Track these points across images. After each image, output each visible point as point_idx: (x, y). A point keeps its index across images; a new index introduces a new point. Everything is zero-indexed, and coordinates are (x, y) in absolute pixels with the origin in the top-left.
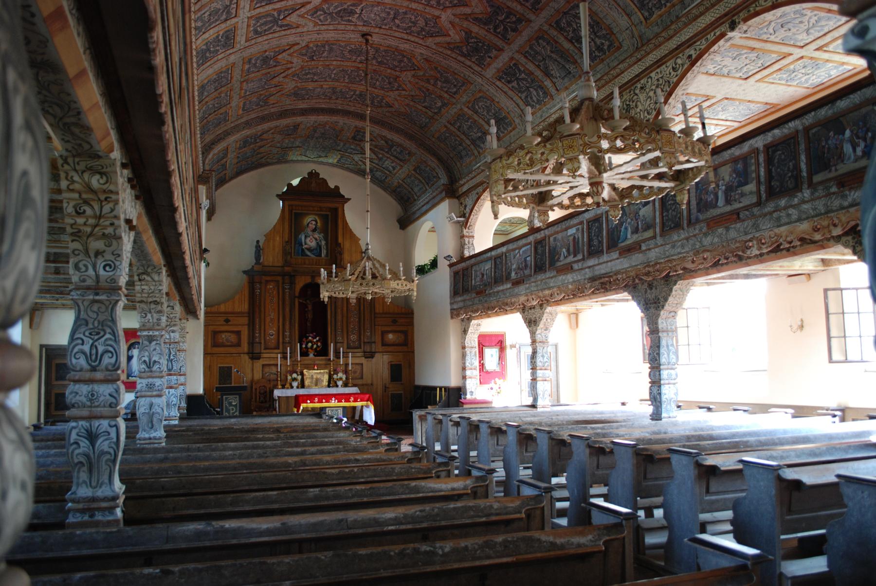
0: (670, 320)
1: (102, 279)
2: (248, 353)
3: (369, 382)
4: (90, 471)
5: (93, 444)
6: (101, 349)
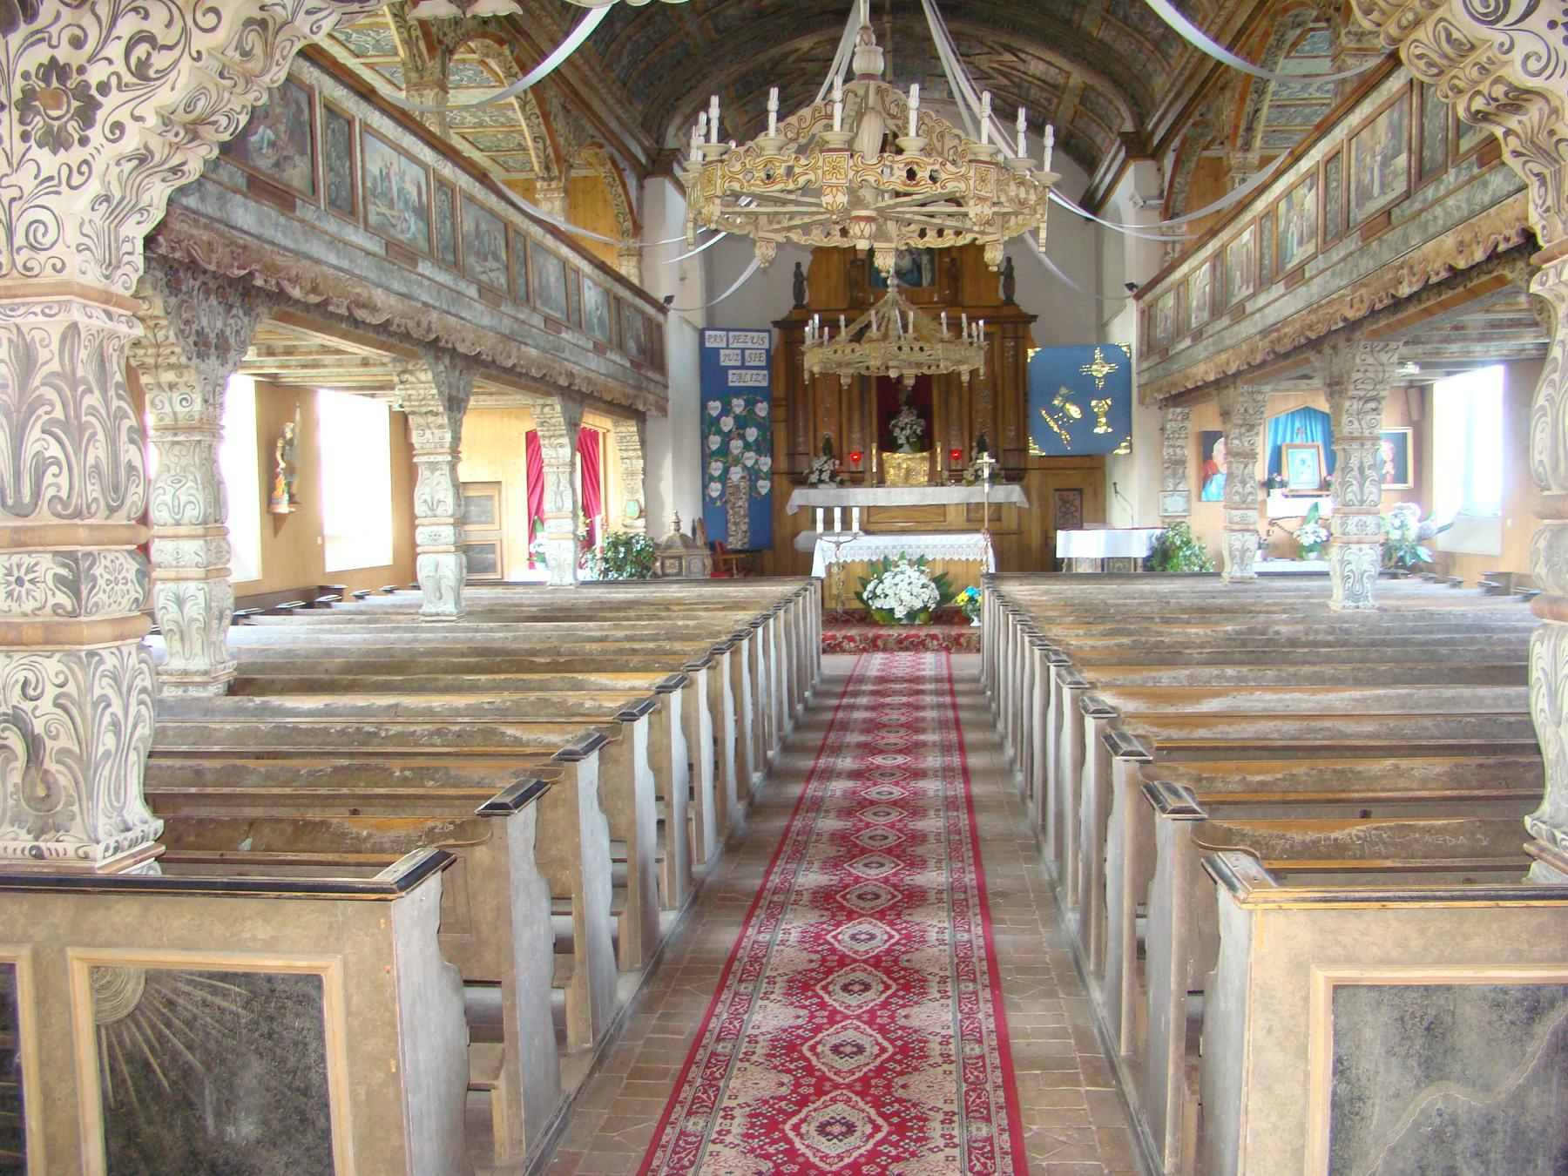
0: (1369, 417)
1: (180, 417)
2: (788, 473)
3: (1014, 526)
4: (182, 639)
5: (181, 608)
6: (183, 499)
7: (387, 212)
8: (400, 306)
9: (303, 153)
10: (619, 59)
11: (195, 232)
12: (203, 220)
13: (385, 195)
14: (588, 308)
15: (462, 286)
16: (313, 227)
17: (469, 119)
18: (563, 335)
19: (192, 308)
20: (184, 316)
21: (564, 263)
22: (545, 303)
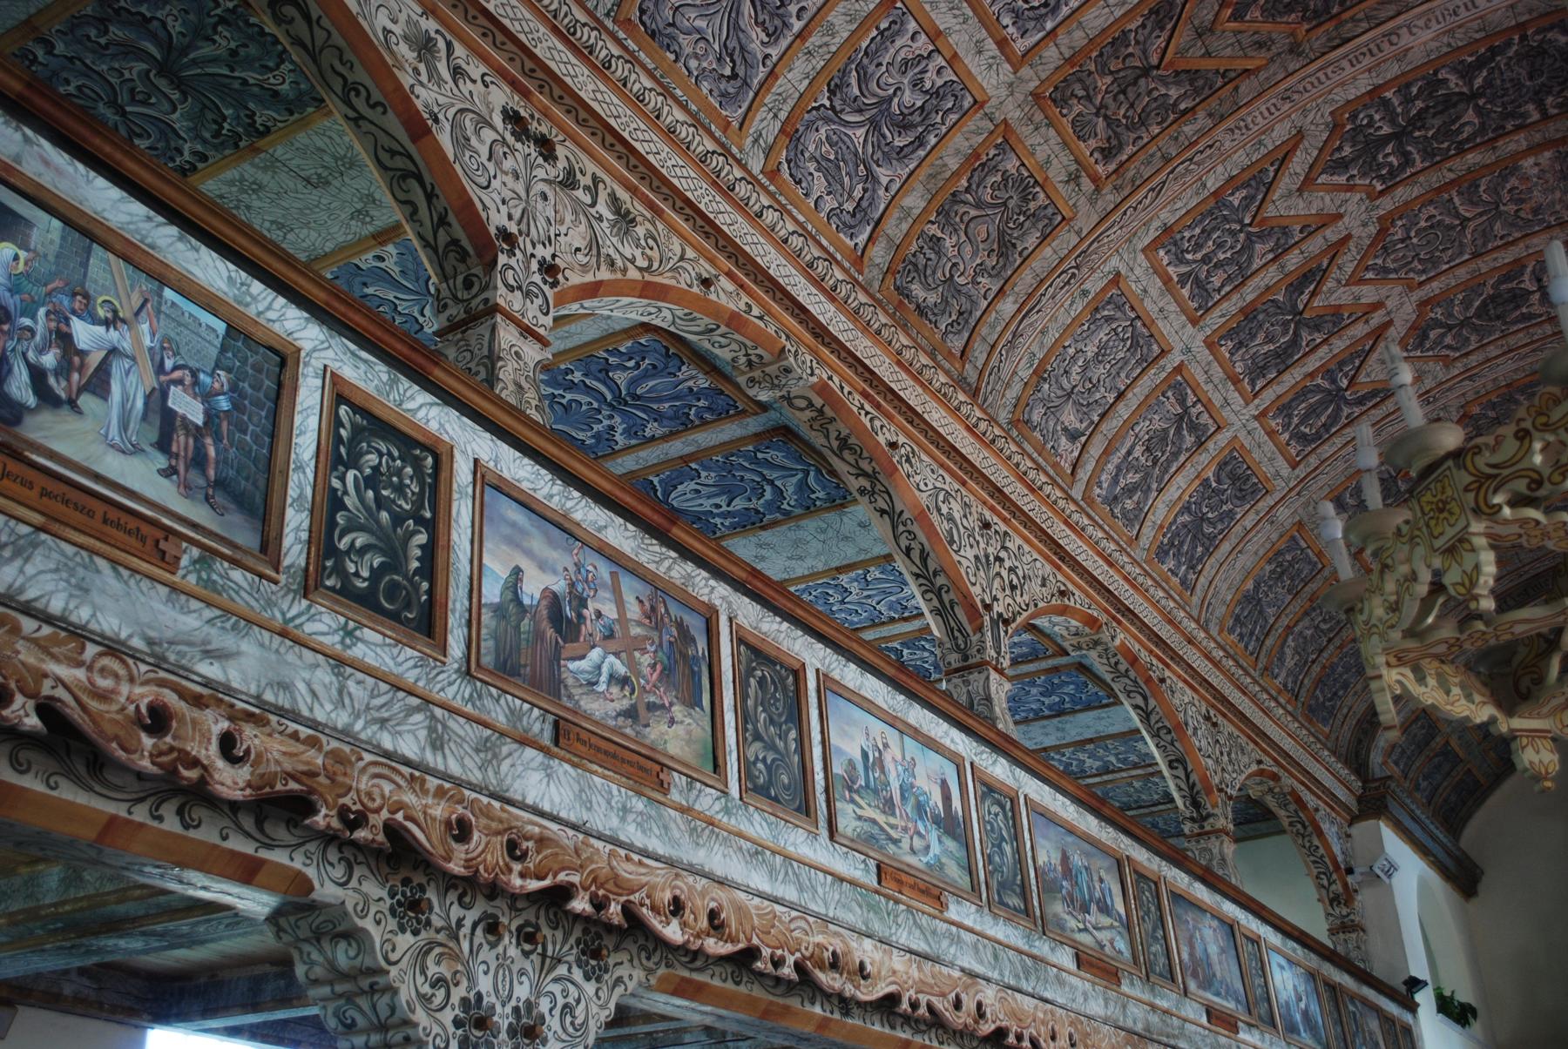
7: (881, 819)
8: (915, 974)
9: (693, 702)
10: (1281, 659)
11: (409, 798)
12: (432, 783)
13: (877, 791)
14: (1283, 996)
15: (1042, 947)
16: (711, 823)
17: (1089, 762)
18: (1242, 1035)
19: (456, 957)
20: (433, 970)
21: (1230, 927)
22: (1207, 984)
